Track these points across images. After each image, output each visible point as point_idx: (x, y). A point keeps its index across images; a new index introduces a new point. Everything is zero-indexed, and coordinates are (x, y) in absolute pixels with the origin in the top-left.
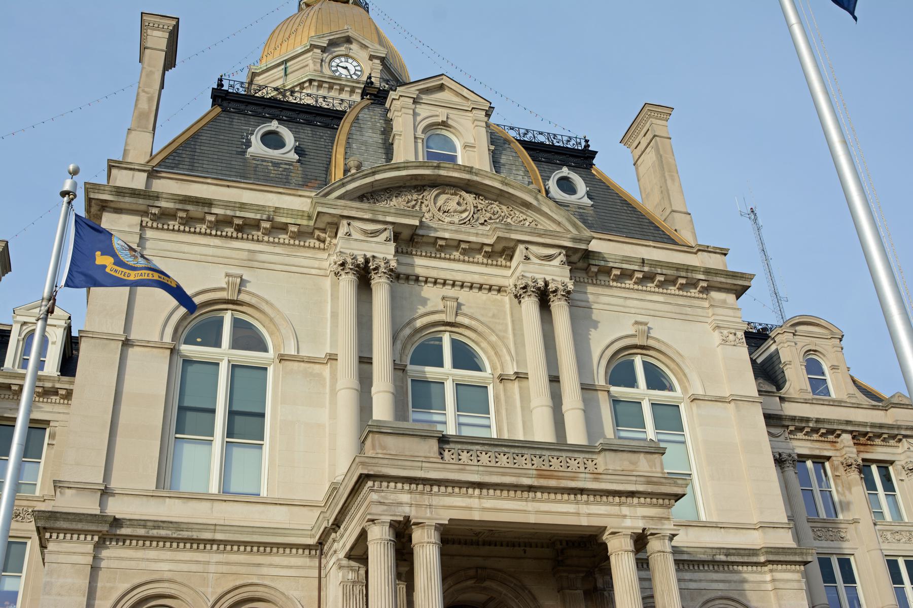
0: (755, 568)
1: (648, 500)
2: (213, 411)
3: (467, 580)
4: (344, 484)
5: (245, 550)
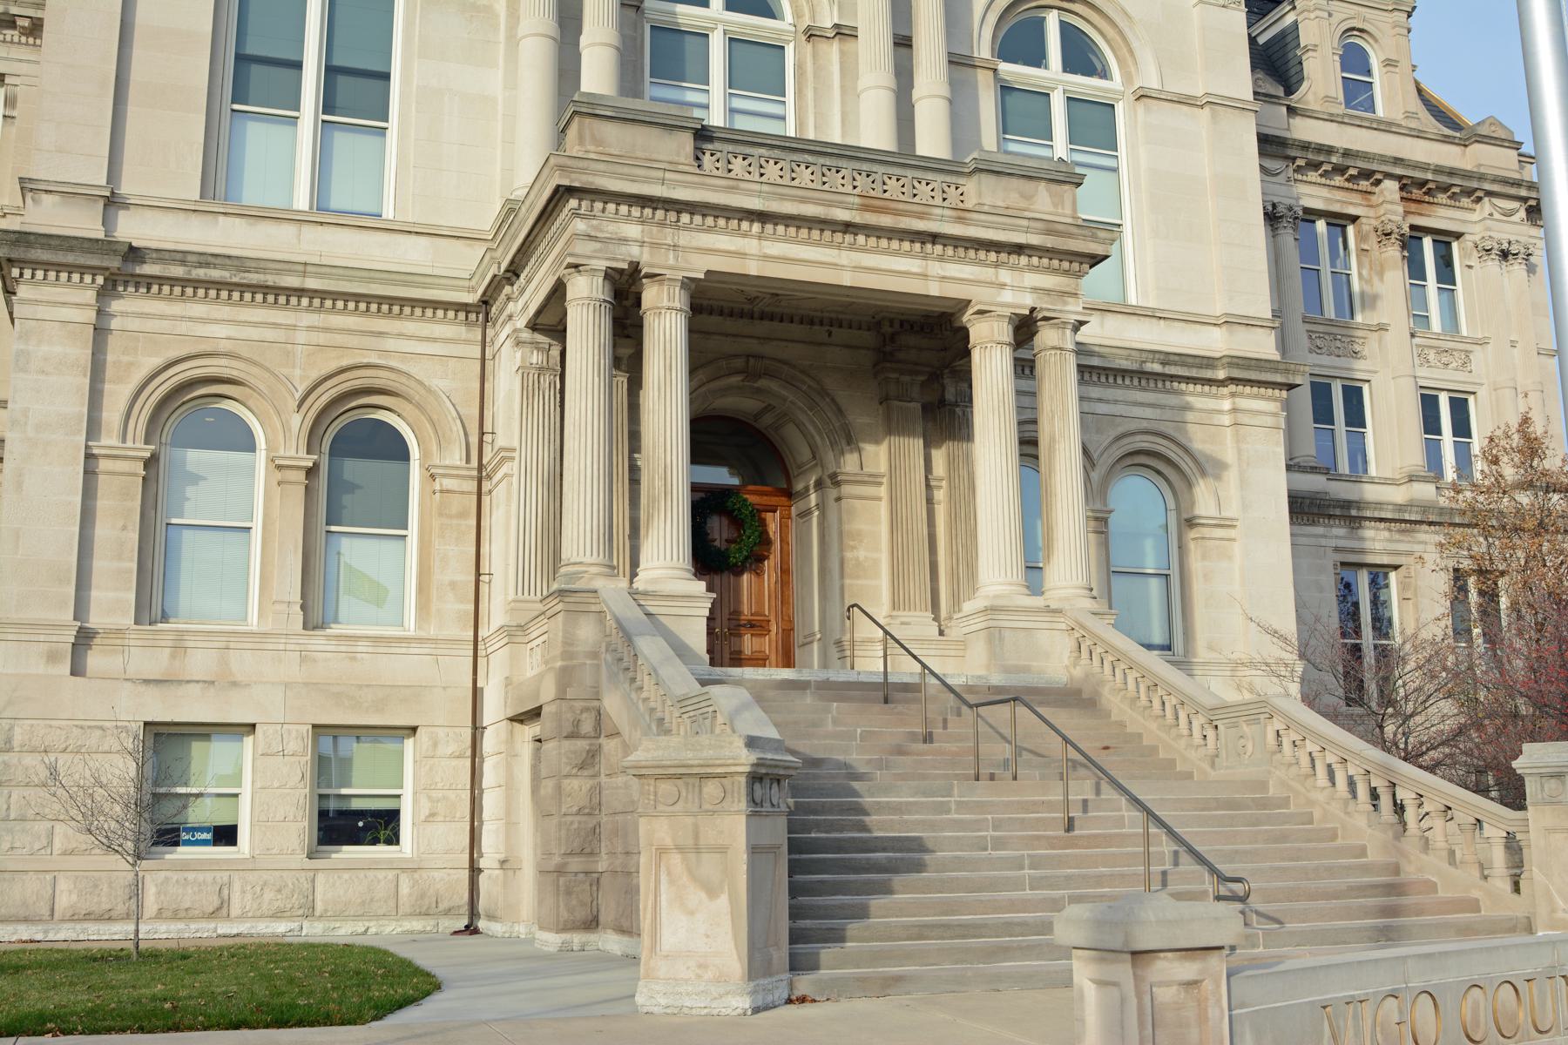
0: (1207, 388)
1: (1045, 261)
2: (298, 65)
3: (729, 375)
4: (527, 203)
5: (357, 308)
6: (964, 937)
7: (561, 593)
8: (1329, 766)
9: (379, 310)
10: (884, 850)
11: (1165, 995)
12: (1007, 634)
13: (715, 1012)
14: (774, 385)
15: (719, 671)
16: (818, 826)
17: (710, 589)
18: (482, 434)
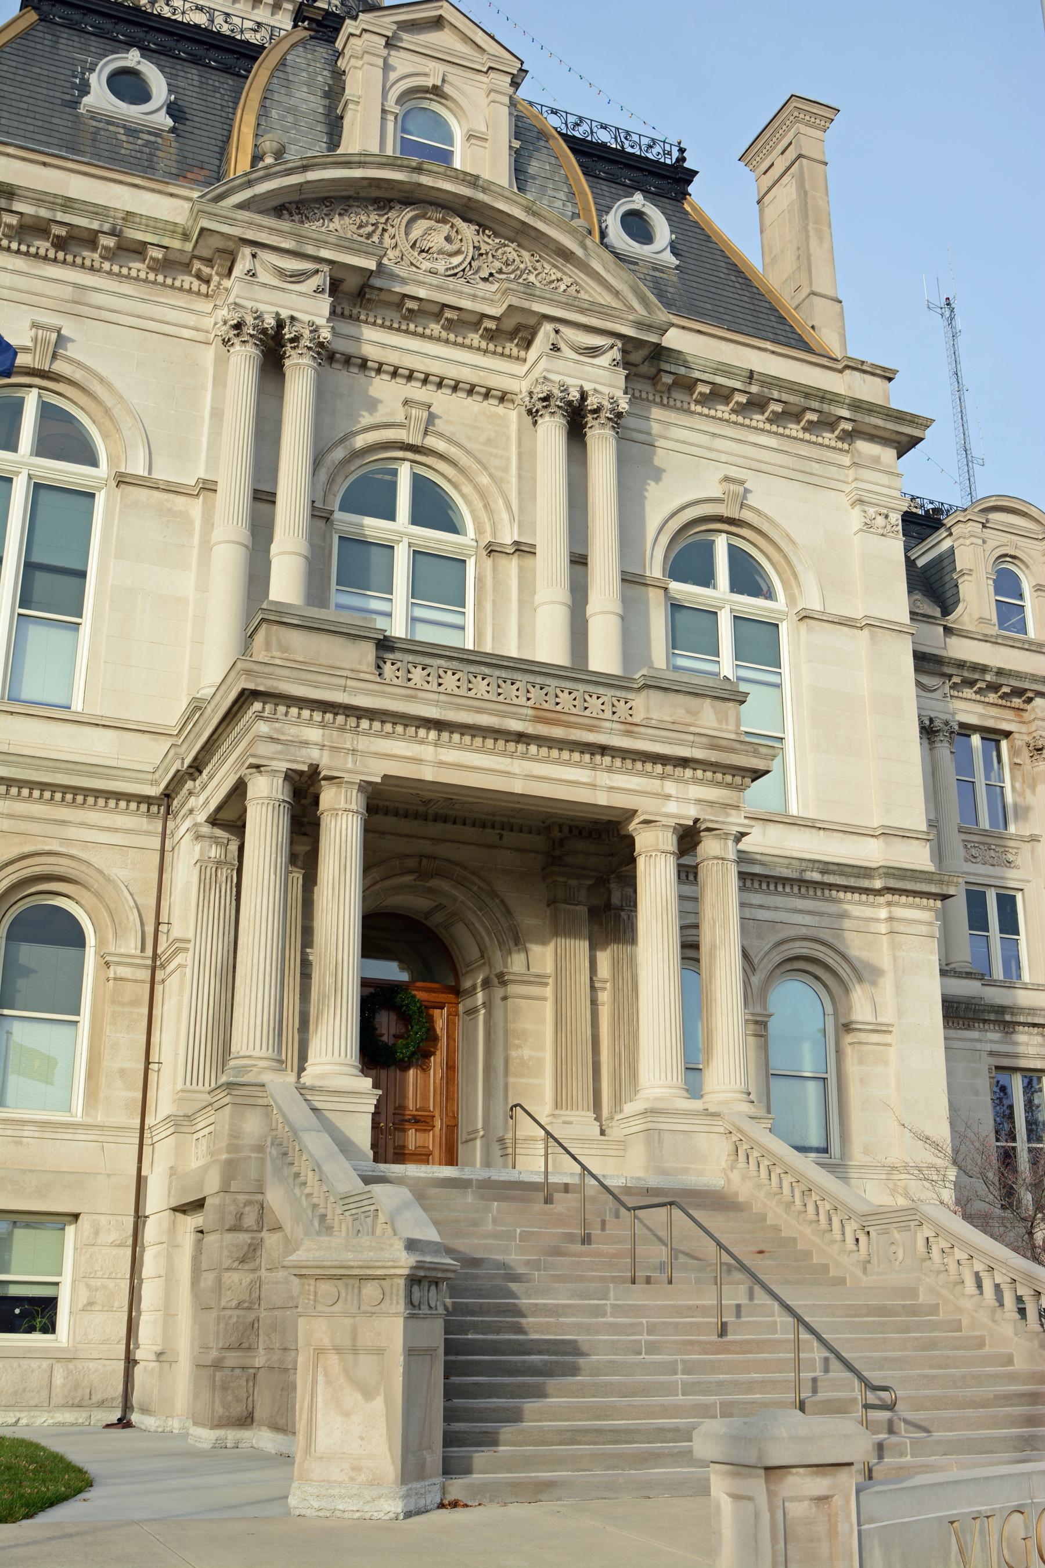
0: (864, 897)
4: (213, 703)
6: (616, 1442)
7: (230, 1085)
8: (977, 1274)
9: (63, 799)
10: (540, 1353)
11: (798, 1510)
12: (666, 1137)
13: (367, 1516)
14: (444, 885)
15: (384, 1168)
16: (475, 1327)
17: (376, 1086)
18: (158, 923)
